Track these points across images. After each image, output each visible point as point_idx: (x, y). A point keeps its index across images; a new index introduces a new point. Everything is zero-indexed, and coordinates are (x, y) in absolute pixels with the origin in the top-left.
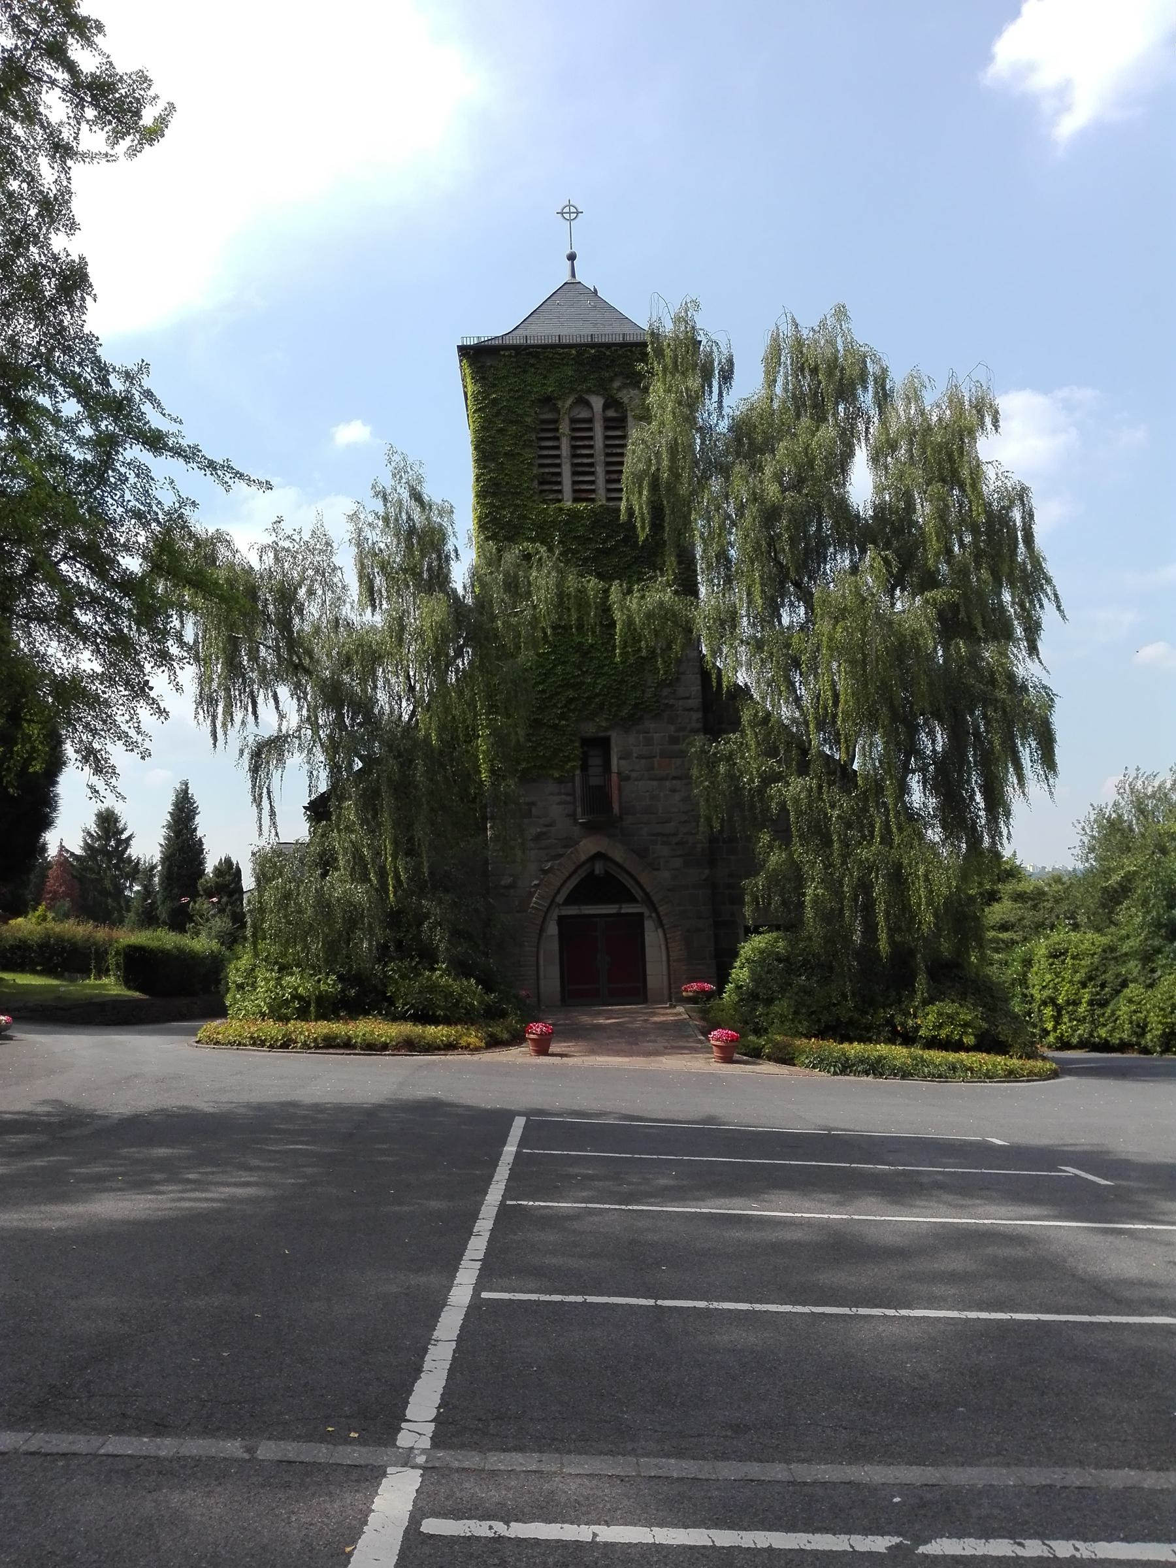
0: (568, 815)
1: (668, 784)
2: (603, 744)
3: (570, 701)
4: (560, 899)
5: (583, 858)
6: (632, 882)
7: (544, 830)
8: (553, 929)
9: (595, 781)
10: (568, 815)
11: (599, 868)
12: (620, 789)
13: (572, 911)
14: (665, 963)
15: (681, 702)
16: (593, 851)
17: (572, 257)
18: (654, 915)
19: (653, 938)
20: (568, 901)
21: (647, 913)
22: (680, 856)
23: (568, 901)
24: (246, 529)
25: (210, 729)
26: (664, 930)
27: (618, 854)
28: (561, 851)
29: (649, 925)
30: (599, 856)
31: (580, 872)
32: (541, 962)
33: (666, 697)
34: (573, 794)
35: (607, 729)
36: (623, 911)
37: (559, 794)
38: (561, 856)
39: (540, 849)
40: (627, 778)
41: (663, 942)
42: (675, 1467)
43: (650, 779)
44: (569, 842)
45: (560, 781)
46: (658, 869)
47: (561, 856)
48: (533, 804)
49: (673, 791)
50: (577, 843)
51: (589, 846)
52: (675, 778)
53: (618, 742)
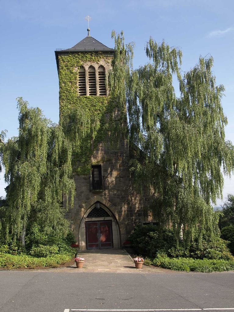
6: (108, 210)
11: (98, 206)
13: (90, 219)
14: (119, 236)
17: (88, 30)
18: (115, 220)
21: (113, 220)
23: (88, 217)
26: (118, 225)
30: (98, 202)
31: (92, 207)
36: (106, 219)
41: (118, 229)
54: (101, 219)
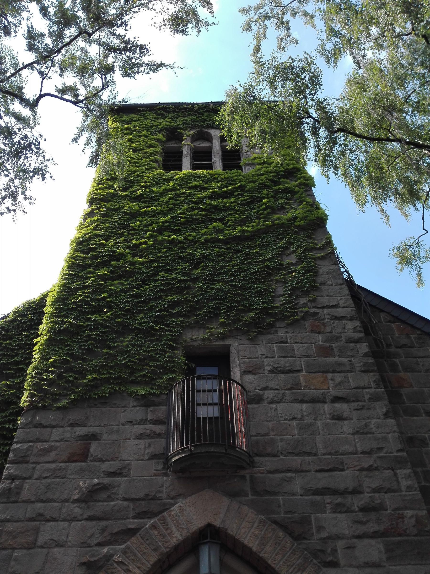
0: (154, 457)
2: (220, 360)
3: (174, 304)
5: (177, 537)
7: (107, 481)
10: (154, 457)
12: (248, 417)
15: (326, 311)
16: (198, 523)
22: (374, 535)
24: (27, 97)
25: (52, 93)
28: (132, 524)
33: (305, 305)
34: (164, 422)
35: (223, 337)
37: (143, 422)
38: (131, 532)
39: (91, 518)
42: (100, 556)
43: (295, 401)
44: (151, 507)
45: (146, 402)
47: (131, 532)
48: (94, 437)
49: (339, 418)
50: (166, 508)
52: (337, 399)
53: (240, 352)
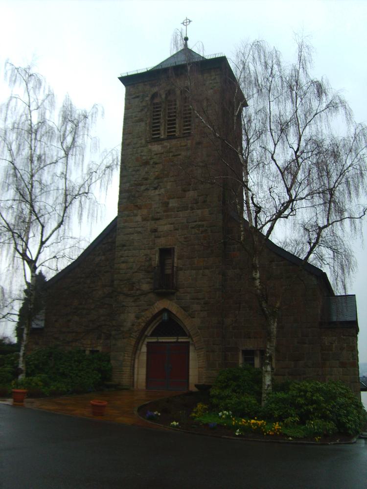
1: (201, 271)
4: (149, 331)
5: (156, 311)
8: (144, 349)
9: (168, 272)
16: (162, 307)
19: (192, 355)
20: (152, 335)
27: (174, 308)
29: (191, 348)
30: (165, 310)
32: (136, 366)
36: (179, 340)
38: (146, 310)
39: (137, 306)
40: (181, 269)
46: (194, 318)
51: (160, 305)
54: (172, 340)
